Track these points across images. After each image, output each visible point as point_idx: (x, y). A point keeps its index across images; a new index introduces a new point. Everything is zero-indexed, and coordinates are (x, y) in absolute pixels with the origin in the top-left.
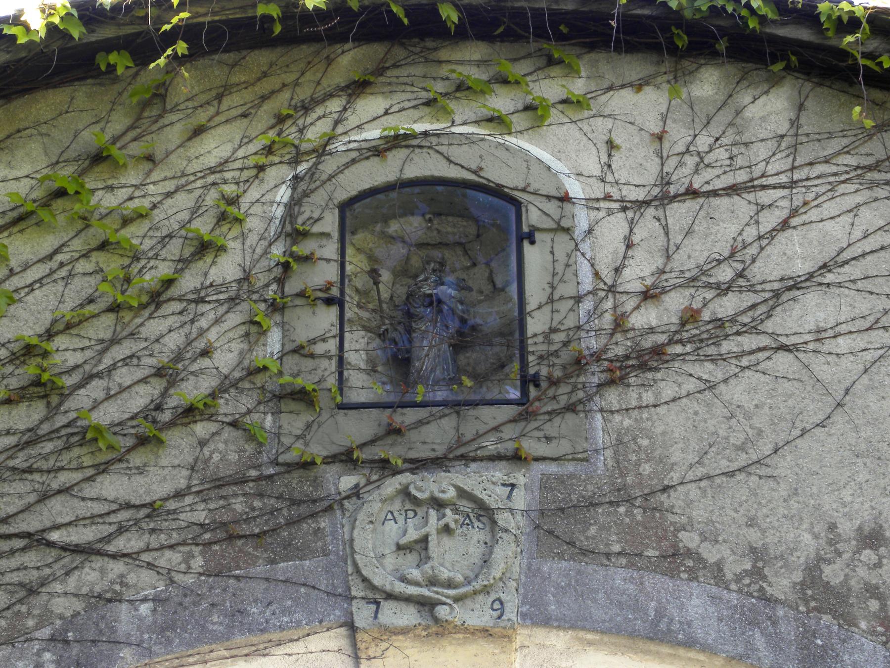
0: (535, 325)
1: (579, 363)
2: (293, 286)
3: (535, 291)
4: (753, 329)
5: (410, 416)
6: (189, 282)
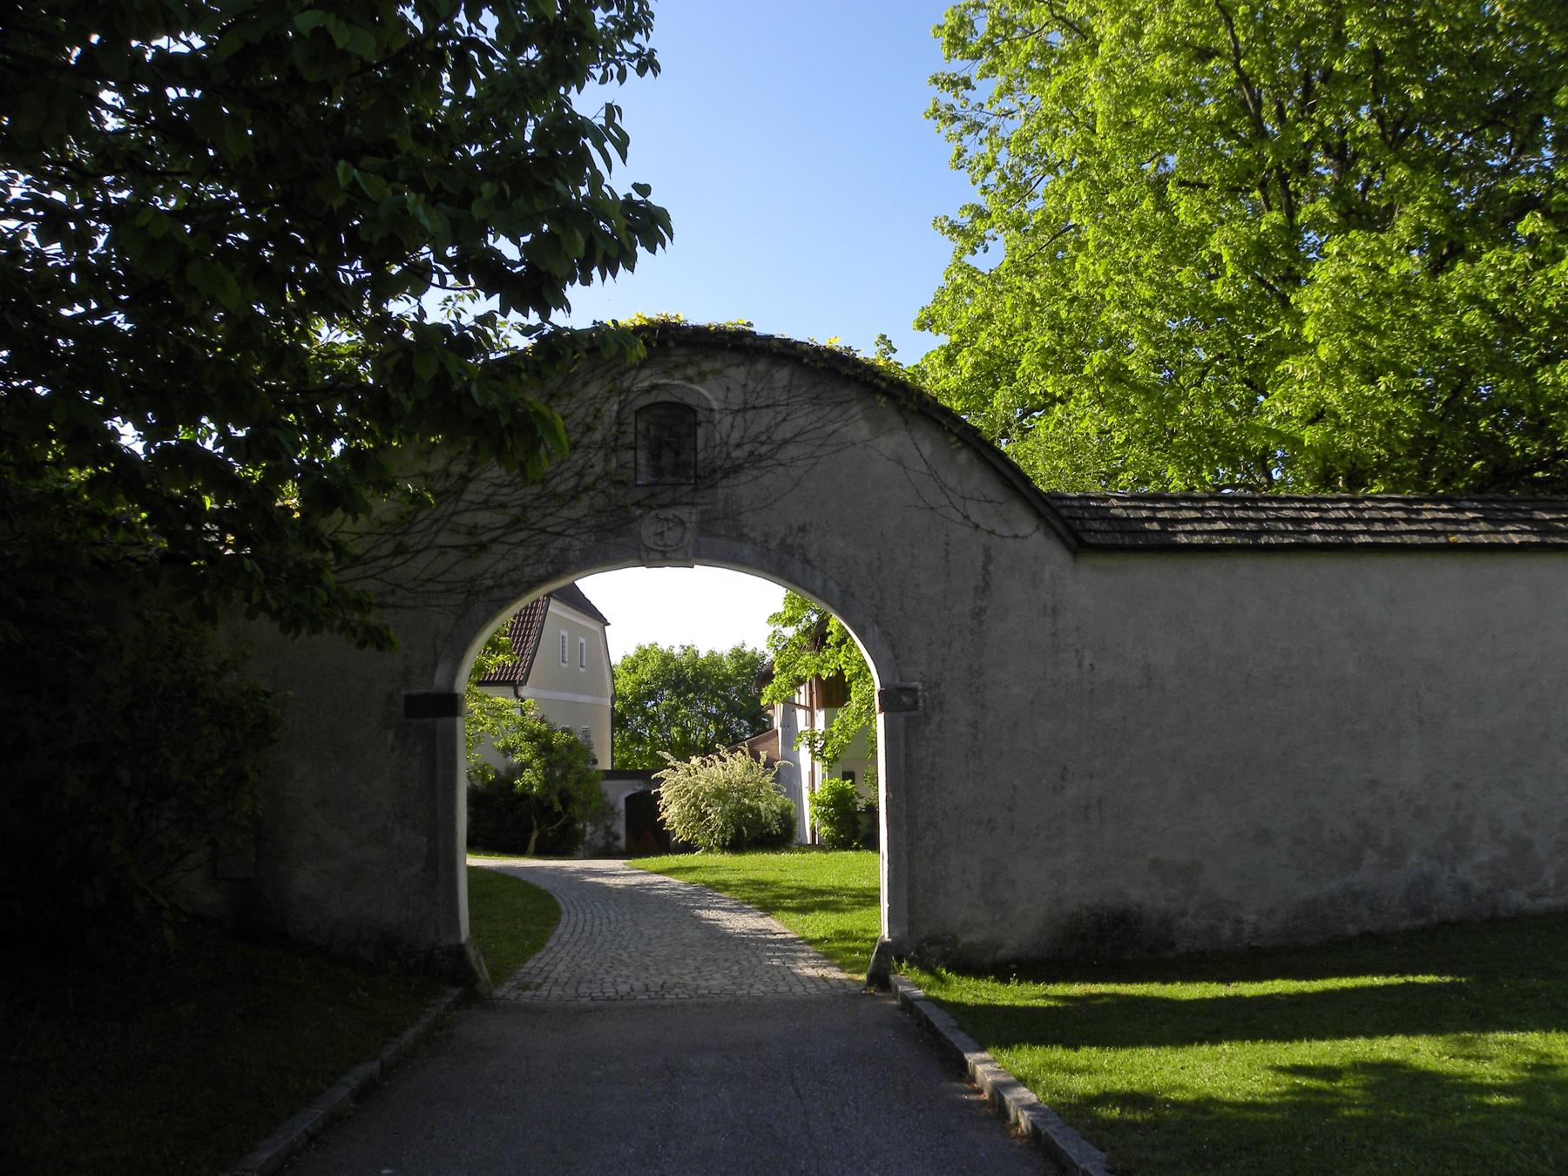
0: (701, 457)
1: (714, 471)
2: (620, 442)
3: (700, 444)
4: (771, 458)
5: (658, 489)
6: (585, 441)
